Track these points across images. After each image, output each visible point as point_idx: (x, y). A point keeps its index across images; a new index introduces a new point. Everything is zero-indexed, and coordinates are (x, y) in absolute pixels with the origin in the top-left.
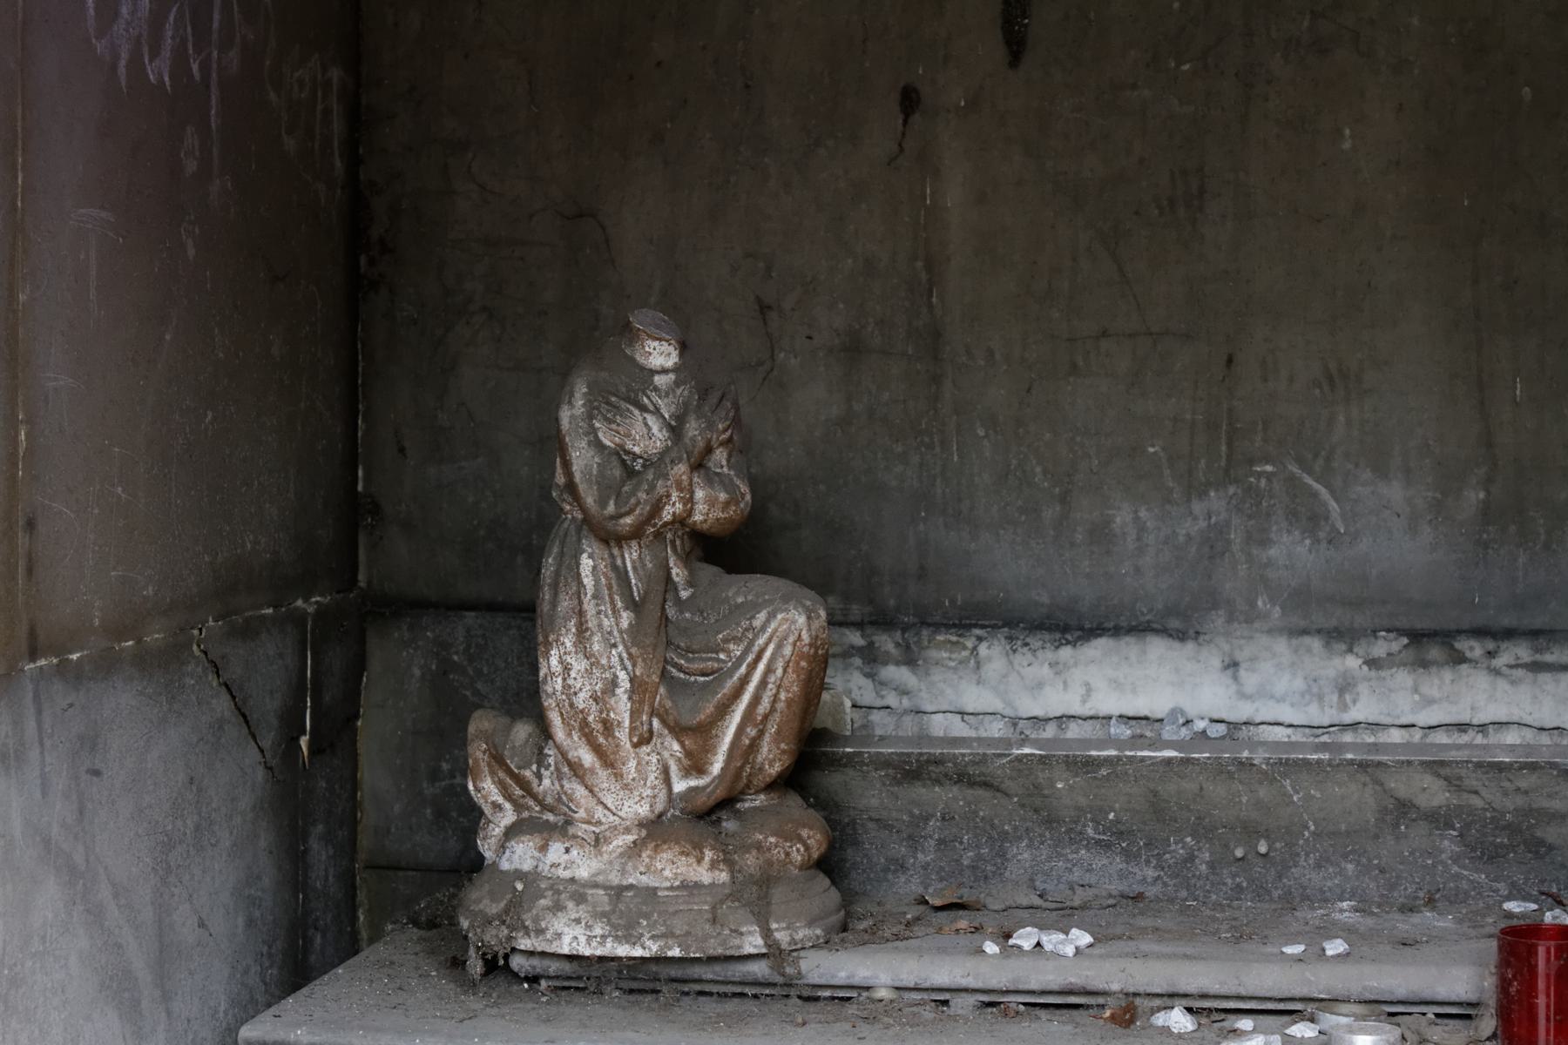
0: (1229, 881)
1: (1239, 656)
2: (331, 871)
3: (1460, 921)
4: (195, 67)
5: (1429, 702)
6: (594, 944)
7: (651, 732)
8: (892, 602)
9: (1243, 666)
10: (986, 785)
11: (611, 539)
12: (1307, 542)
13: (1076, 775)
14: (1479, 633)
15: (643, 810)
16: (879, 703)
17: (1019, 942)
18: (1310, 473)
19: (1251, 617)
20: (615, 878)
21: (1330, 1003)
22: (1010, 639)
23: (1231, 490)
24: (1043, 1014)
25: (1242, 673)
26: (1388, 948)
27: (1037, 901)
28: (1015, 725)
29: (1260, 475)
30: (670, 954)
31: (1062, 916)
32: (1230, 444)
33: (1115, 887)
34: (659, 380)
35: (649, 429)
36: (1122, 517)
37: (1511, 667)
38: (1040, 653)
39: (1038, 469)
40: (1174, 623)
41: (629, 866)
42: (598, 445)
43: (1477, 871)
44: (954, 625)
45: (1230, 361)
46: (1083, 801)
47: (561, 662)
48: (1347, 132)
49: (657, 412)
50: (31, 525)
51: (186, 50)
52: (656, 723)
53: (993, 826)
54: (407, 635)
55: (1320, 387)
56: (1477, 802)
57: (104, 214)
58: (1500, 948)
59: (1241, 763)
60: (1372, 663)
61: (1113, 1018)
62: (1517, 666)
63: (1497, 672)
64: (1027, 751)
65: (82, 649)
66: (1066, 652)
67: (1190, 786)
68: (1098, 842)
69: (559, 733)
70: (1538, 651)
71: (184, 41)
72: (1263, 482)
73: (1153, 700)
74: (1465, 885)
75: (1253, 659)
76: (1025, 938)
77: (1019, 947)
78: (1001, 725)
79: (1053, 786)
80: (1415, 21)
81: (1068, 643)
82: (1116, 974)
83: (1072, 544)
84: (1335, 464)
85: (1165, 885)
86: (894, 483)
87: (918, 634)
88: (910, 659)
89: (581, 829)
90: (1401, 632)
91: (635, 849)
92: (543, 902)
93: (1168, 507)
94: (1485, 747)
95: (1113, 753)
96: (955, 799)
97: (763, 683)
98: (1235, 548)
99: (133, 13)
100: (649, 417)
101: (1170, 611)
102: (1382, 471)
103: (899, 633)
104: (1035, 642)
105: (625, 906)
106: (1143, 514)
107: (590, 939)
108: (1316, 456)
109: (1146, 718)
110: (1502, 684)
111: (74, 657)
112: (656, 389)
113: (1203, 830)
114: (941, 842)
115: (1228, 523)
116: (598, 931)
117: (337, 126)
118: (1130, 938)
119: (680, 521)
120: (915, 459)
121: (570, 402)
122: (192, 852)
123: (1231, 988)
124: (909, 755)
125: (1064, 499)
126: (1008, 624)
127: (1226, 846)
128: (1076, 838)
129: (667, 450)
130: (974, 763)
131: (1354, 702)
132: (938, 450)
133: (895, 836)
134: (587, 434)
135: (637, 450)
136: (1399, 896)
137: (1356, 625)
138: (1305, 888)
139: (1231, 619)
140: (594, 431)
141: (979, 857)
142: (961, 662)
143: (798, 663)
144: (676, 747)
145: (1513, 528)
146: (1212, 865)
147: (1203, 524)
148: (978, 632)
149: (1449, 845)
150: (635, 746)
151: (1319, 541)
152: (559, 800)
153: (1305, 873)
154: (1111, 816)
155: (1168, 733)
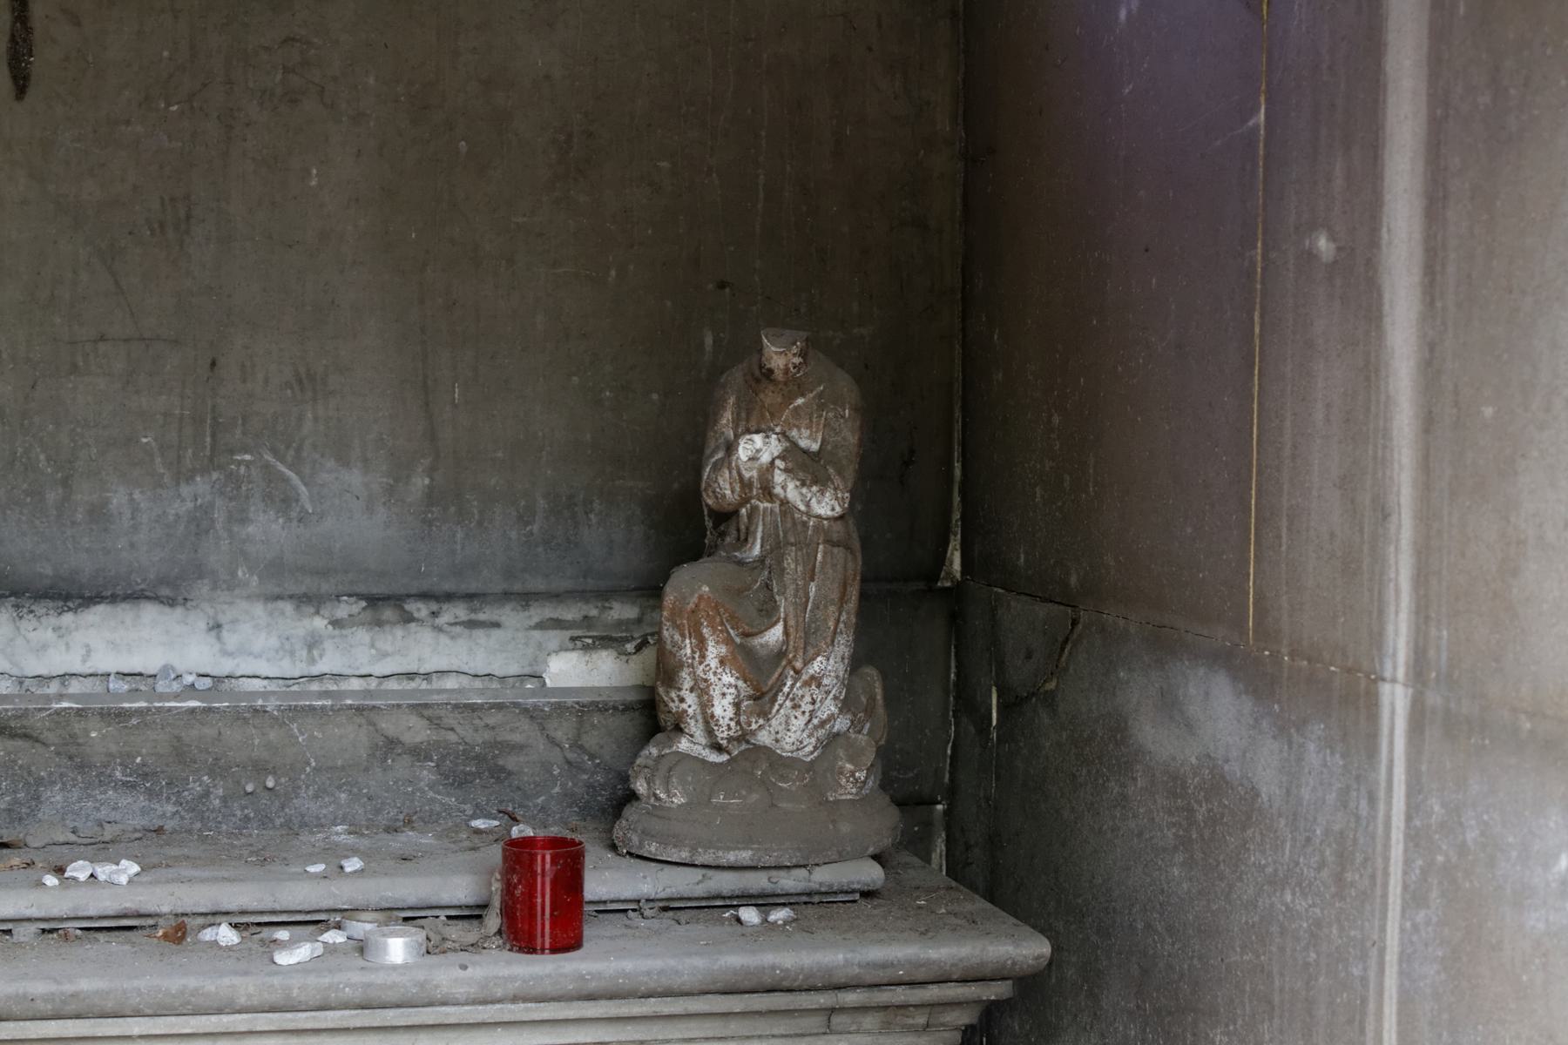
0: (239, 813)
1: (222, 619)
3: (438, 837)
5: (385, 655)
9: (226, 627)
10: (26, 736)
14: (425, 596)
17: (75, 874)
18: (283, 461)
19: (232, 585)
21: (352, 912)
22: (17, 607)
23: (215, 475)
24: (101, 936)
25: (225, 634)
26: (392, 863)
27: (73, 838)
28: (21, 683)
29: (239, 463)
31: (103, 848)
32: (213, 436)
33: (139, 822)
36: (118, 499)
37: (451, 624)
38: (43, 620)
39: (42, 457)
40: (165, 591)
43: (449, 795)
45: (213, 364)
46: (113, 748)
53: (30, 773)
55: (292, 388)
56: (452, 737)
58: (505, 859)
59: (256, 711)
60: (336, 623)
61: (165, 936)
62: (456, 624)
63: (439, 629)
64: (65, 705)
66: (68, 618)
67: (210, 732)
68: (125, 784)
70: (474, 611)
72: (243, 469)
73: (146, 659)
74: (437, 808)
75: (234, 621)
76: (79, 870)
77: (74, 879)
78: (9, 683)
80: (371, 81)
81: (70, 609)
82: (164, 898)
83: (73, 523)
84: (305, 454)
85: (182, 818)
90: (360, 596)
93: (159, 491)
94: (431, 692)
95: (144, 704)
98: (218, 526)
101: (163, 581)
102: (344, 462)
104: (40, 609)
106: (137, 495)
108: (288, 447)
109: (140, 674)
110: (444, 639)
113: (218, 769)
115: (212, 505)
118: (168, 866)
123: (268, 904)
125: (65, 482)
126: (14, 594)
127: (238, 783)
128: (104, 780)
130: (16, 717)
131: (321, 656)
136: (382, 820)
138: (303, 816)
139: (214, 588)
141: (16, 801)
145: (452, 509)
146: (224, 799)
147: (190, 505)
149: (427, 774)
153: (304, 803)
154: (139, 760)
155: (161, 686)
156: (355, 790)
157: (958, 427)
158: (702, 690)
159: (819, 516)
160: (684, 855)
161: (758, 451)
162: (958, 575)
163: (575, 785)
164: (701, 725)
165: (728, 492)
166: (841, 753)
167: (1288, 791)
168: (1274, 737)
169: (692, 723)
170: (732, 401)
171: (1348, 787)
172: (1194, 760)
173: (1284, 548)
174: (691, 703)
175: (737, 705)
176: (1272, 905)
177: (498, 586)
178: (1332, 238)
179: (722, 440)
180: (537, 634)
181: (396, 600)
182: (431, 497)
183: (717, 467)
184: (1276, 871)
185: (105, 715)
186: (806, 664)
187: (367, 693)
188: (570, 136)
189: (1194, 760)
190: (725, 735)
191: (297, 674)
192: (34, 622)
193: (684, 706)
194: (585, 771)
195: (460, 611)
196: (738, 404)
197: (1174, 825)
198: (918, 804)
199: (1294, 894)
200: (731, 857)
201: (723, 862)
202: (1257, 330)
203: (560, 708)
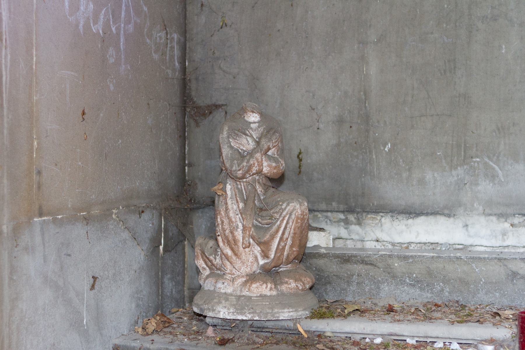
1: (468, 223)
2: (174, 290)
4: (114, 29)
6: (230, 315)
7: (250, 243)
8: (353, 204)
9: (470, 226)
10: (371, 264)
11: (236, 179)
12: (491, 184)
13: (402, 261)
15: (248, 270)
16: (349, 237)
18: (492, 161)
20: (238, 293)
22: (392, 216)
23: (465, 167)
25: (469, 228)
29: (475, 162)
30: (255, 319)
32: (465, 152)
34: (252, 126)
35: (248, 142)
36: (429, 176)
38: (402, 221)
39: (401, 160)
40: (446, 212)
41: (243, 290)
42: (231, 147)
44: (374, 212)
46: (404, 270)
47: (221, 220)
48: (504, 46)
49: (251, 136)
50: (39, 173)
51: (109, 22)
52: (251, 240)
53: (375, 278)
54: (201, 215)
55: (495, 132)
57: (73, 73)
59: (457, 258)
60: (512, 225)
65: (63, 214)
66: (410, 221)
67: (441, 266)
68: (411, 284)
69: (221, 244)
71: (108, 20)
72: (476, 164)
79: (394, 265)
81: (411, 218)
83: (412, 185)
84: (500, 158)
86: (354, 165)
87: (362, 215)
88: (359, 223)
89: (228, 277)
91: (245, 283)
92: (215, 300)
96: (362, 269)
97: (285, 228)
99: (86, 9)
100: (248, 137)
101: (446, 207)
103: (356, 214)
104: (400, 217)
105: (242, 302)
106: (436, 175)
107: (229, 313)
108: (494, 155)
111: (60, 217)
112: (251, 128)
114: (358, 283)
116: (231, 310)
117: (177, 52)
119: (259, 172)
120: (361, 157)
121: (222, 133)
122: (112, 282)
124: (345, 254)
125: (409, 170)
126: (391, 211)
128: (403, 282)
129: (255, 148)
131: (507, 239)
132: (368, 154)
133: (342, 281)
134: (227, 143)
135: (244, 149)
137: (508, 213)
139: (465, 210)
140: (230, 142)
141: (371, 289)
142: (376, 224)
143: (297, 221)
144: (259, 249)
147: (456, 178)
148: (381, 214)
150: (244, 248)
151: (495, 184)
152: (221, 266)
154: (414, 275)
185: (399, 257)
192: (398, 222)
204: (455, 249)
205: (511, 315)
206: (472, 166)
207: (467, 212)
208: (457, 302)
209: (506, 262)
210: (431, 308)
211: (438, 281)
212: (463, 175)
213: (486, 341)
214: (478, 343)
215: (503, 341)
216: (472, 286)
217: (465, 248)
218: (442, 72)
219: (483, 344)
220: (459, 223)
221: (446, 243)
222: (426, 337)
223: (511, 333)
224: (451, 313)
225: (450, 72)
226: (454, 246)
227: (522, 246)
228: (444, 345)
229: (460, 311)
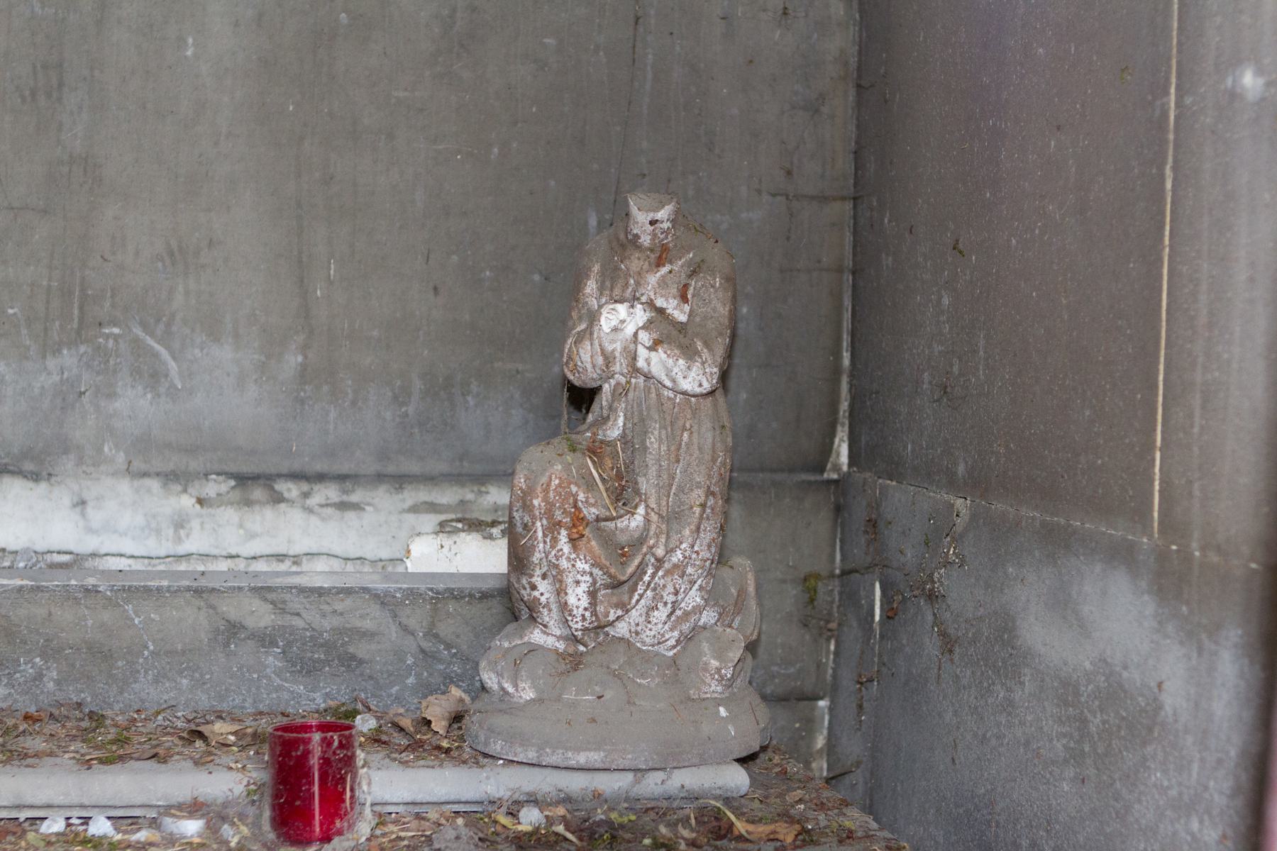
1: (86, 495)
5: (253, 536)
12: (149, 396)
14: (296, 476)
18: (152, 335)
23: (82, 349)
25: (89, 510)
29: (108, 336)
32: (81, 308)
37: (322, 506)
40: (28, 466)
48: (190, 41)
55: (162, 261)
56: (298, 622)
59: (87, 590)
60: (200, 501)
62: (327, 505)
63: (310, 510)
70: (345, 492)
72: (111, 343)
75: (99, 498)
84: (174, 329)
101: (26, 454)
108: (158, 321)
110: (314, 520)
113: (50, 651)
131: (188, 536)
139: (80, 461)
145: (325, 388)
147: (56, 378)
149: (272, 661)
156: (197, 675)
157: (847, 316)
158: (557, 578)
159: (684, 393)
160: (531, 755)
161: (623, 322)
162: (845, 468)
163: (431, 675)
164: (555, 614)
165: (589, 366)
166: (705, 646)
167: (1197, 704)
168: (1181, 643)
169: (545, 612)
170: (596, 268)
171: (607, 367)
172: (1087, 665)
173: (1196, 430)
174: (544, 590)
175: (592, 594)
176: (1175, 833)
177: (371, 467)
178: (1259, 72)
179: (584, 311)
180: (411, 518)
181: (266, 479)
182: (304, 374)
183: (579, 340)
184: (1180, 794)
186: (669, 551)
187: (233, 573)
188: (454, 10)
189: (1087, 665)
190: (579, 626)
191: (163, 553)
193: (536, 593)
194: (440, 661)
195: (330, 492)
196: (602, 273)
197: (1065, 735)
198: (799, 700)
199: (1201, 822)
200: (582, 759)
201: (573, 763)
202: (1169, 185)
203: (412, 594)
204: (52, 566)
205: (232, 733)
206: (99, 348)
207: (84, 468)
208: (79, 705)
209: (213, 599)
210: (16, 726)
211: (30, 651)
212: (75, 371)
213: (180, 807)
214: (160, 814)
215: (226, 805)
216: (120, 664)
217: (77, 561)
218: (27, 93)
219: (174, 816)
220: (63, 496)
221: (26, 550)
222: (19, 807)
223: (245, 782)
224: (74, 738)
225: (49, 95)
226: (48, 558)
227: (224, 553)
228: (69, 825)
229: (94, 730)
